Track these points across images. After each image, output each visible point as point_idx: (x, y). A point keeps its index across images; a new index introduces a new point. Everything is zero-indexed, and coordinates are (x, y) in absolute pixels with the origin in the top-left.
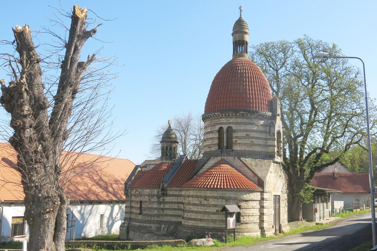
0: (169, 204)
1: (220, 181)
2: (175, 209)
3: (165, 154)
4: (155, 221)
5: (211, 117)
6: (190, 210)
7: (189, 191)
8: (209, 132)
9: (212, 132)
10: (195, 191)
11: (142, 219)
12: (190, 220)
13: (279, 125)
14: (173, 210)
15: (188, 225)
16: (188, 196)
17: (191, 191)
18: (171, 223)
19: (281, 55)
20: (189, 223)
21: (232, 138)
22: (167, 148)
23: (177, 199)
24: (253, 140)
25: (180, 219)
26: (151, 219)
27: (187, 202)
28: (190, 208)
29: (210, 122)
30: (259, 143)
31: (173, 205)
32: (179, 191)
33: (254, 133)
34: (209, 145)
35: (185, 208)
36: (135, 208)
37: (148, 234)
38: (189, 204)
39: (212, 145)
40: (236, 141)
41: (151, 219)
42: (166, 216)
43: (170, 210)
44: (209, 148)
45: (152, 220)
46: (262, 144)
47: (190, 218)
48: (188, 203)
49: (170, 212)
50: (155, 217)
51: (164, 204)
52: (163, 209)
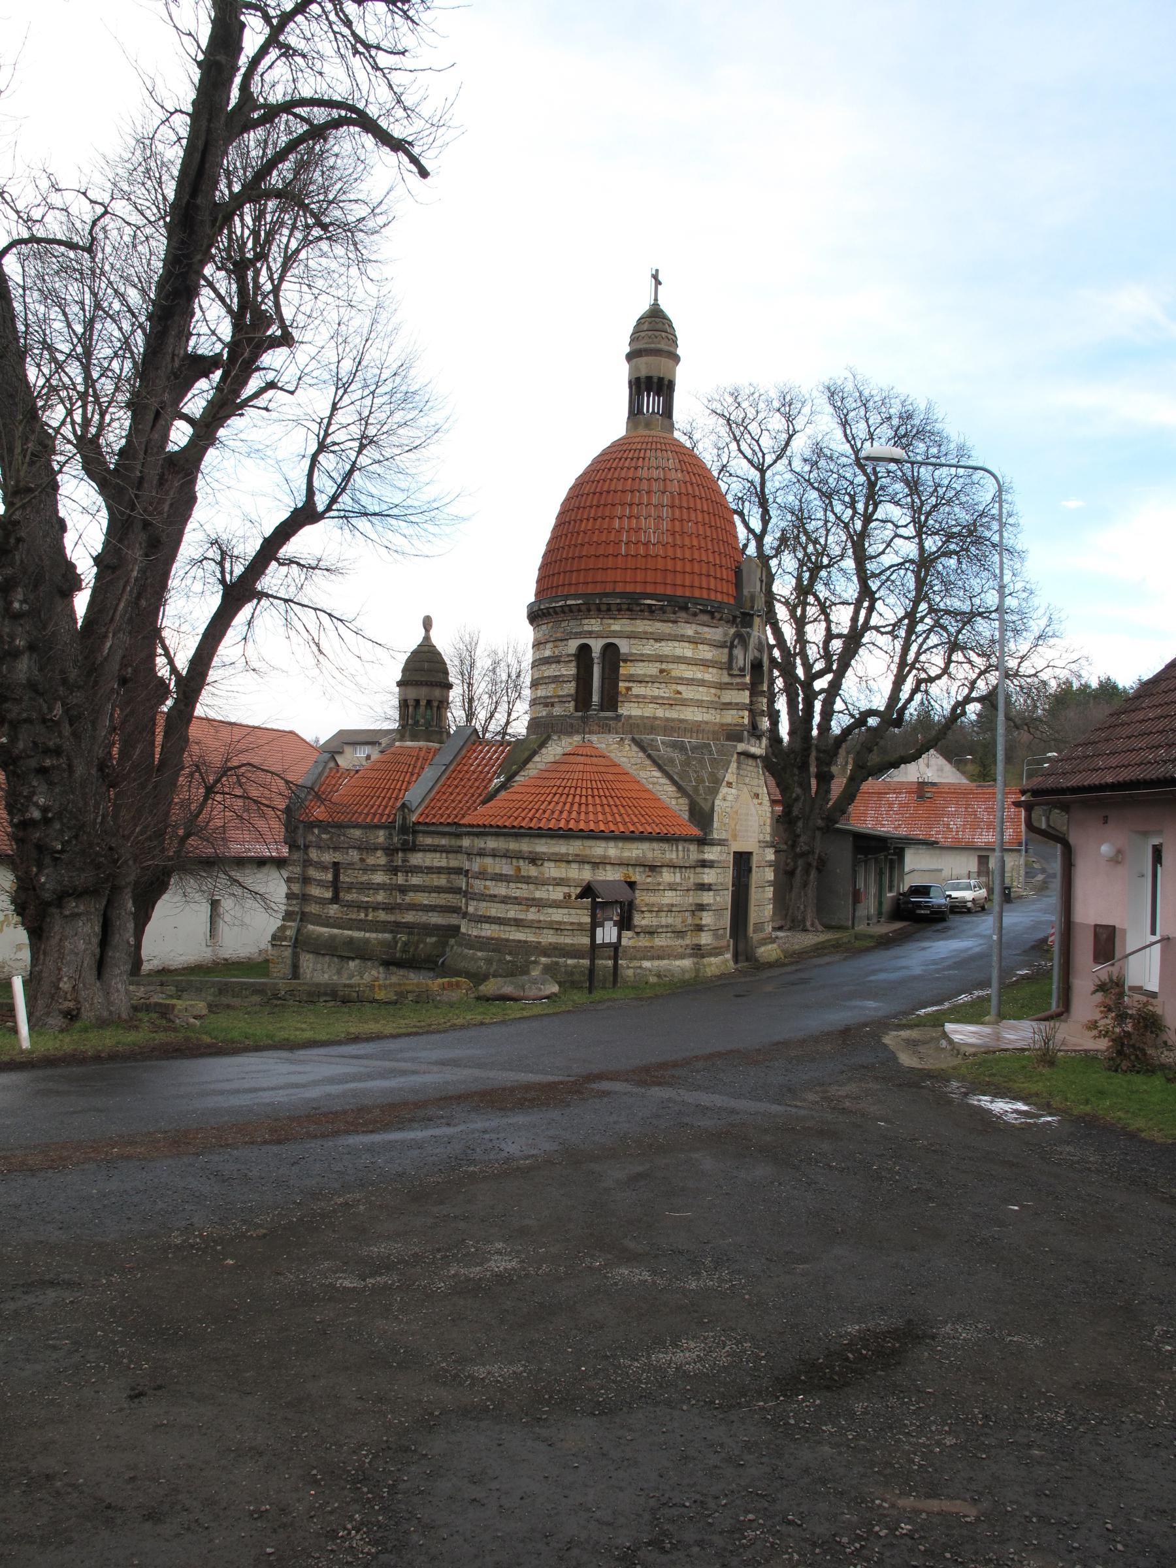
2: (439, 890)
3: (410, 722)
6: (488, 892)
10: (502, 839)
18: (428, 929)
24: (679, 688)
25: (453, 920)
28: (485, 887)
30: (699, 697)
33: (683, 667)
37: (357, 961)
38: (482, 875)
40: (629, 689)
49: (424, 899)
51: (407, 872)
52: (403, 890)
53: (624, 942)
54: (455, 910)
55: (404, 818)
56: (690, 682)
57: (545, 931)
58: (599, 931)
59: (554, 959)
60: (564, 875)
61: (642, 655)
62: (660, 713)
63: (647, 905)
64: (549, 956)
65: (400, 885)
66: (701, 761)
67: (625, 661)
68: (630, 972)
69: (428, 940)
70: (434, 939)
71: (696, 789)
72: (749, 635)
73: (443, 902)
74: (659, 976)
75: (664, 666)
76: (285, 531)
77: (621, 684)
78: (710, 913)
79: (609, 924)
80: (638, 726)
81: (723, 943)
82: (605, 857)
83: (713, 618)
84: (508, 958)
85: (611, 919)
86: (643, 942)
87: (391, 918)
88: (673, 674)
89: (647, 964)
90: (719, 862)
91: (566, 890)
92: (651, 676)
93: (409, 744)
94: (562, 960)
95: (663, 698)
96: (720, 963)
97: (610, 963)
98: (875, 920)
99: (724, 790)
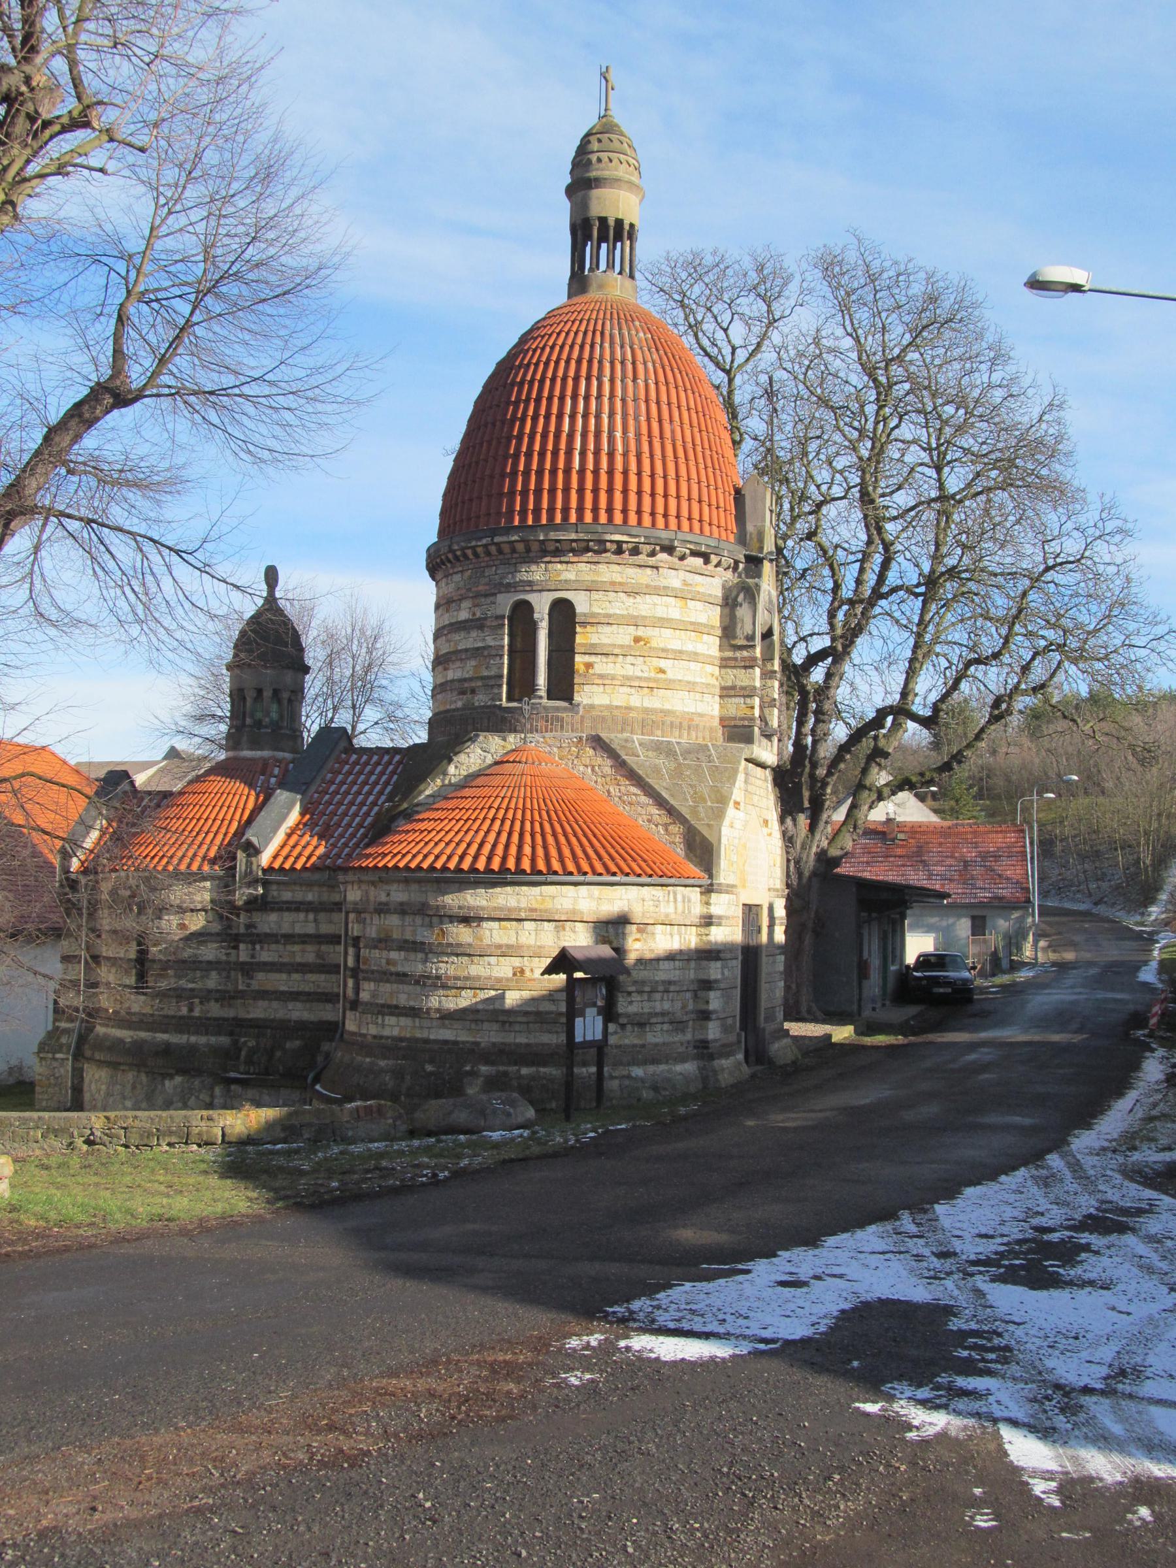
0: (277, 942)
1: (528, 839)
2: (303, 968)
3: (248, 721)
4: (208, 1019)
5: (476, 555)
6: (393, 969)
7: (386, 887)
8: (466, 621)
9: (476, 624)
10: (414, 887)
11: (148, 1010)
12: (391, 1014)
13: (771, 602)
14: (297, 971)
15: (381, 1037)
16: (382, 909)
17: (395, 886)
18: (286, 1028)
19: (752, 306)
20: (383, 1026)
21: (571, 652)
22: (260, 692)
23: (315, 920)
24: (663, 664)
25: (326, 1013)
26: (191, 1010)
27: (372, 932)
28: (388, 962)
29: (470, 578)
30: (689, 678)
31: (296, 948)
32: (321, 885)
33: (667, 633)
34: (465, 680)
35: (366, 961)
36: (113, 965)
37: (178, 1079)
38: (384, 942)
39: (479, 683)
40: (589, 666)
41: (191, 1010)
42: (263, 999)
43: (281, 971)
44: (463, 693)
45: (199, 1018)
46: (698, 680)
47: (389, 1006)
48: (380, 941)
49: (281, 982)
50: (212, 1003)
51: (253, 943)
52: (248, 969)
53: (612, 1040)
54: (329, 998)
55: (249, 864)
56: (678, 655)
57: (486, 1025)
58: (579, 1021)
59: (501, 1068)
60: (513, 941)
61: (608, 616)
62: (636, 700)
63: (635, 982)
64: (493, 1064)
65: (243, 963)
66: (697, 770)
67: (584, 624)
68: (615, 1084)
69: (288, 1045)
70: (298, 1043)
71: (694, 810)
72: (758, 586)
73: (307, 988)
74: (655, 1088)
75: (641, 632)
76: (82, 416)
77: (578, 659)
78: (718, 993)
79: (591, 1012)
80: (604, 719)
81: (732, 1038)
82: (574, 911)
83: (707, 561)
84: (429, 1068)
85: (594, 1005)
86: (630, 1038)
87: (230, 1013)
88: (654, 644)
89: (637, 1072)
90: (727, 918)
91: (516, 962)
92: (622, 646)
93: (247, 753)
94: (512, 1069)
95: (640, 678)
96: (731, 1067)
97: (593, 1069)
98: (879, 1005)
99: (731, 812)
